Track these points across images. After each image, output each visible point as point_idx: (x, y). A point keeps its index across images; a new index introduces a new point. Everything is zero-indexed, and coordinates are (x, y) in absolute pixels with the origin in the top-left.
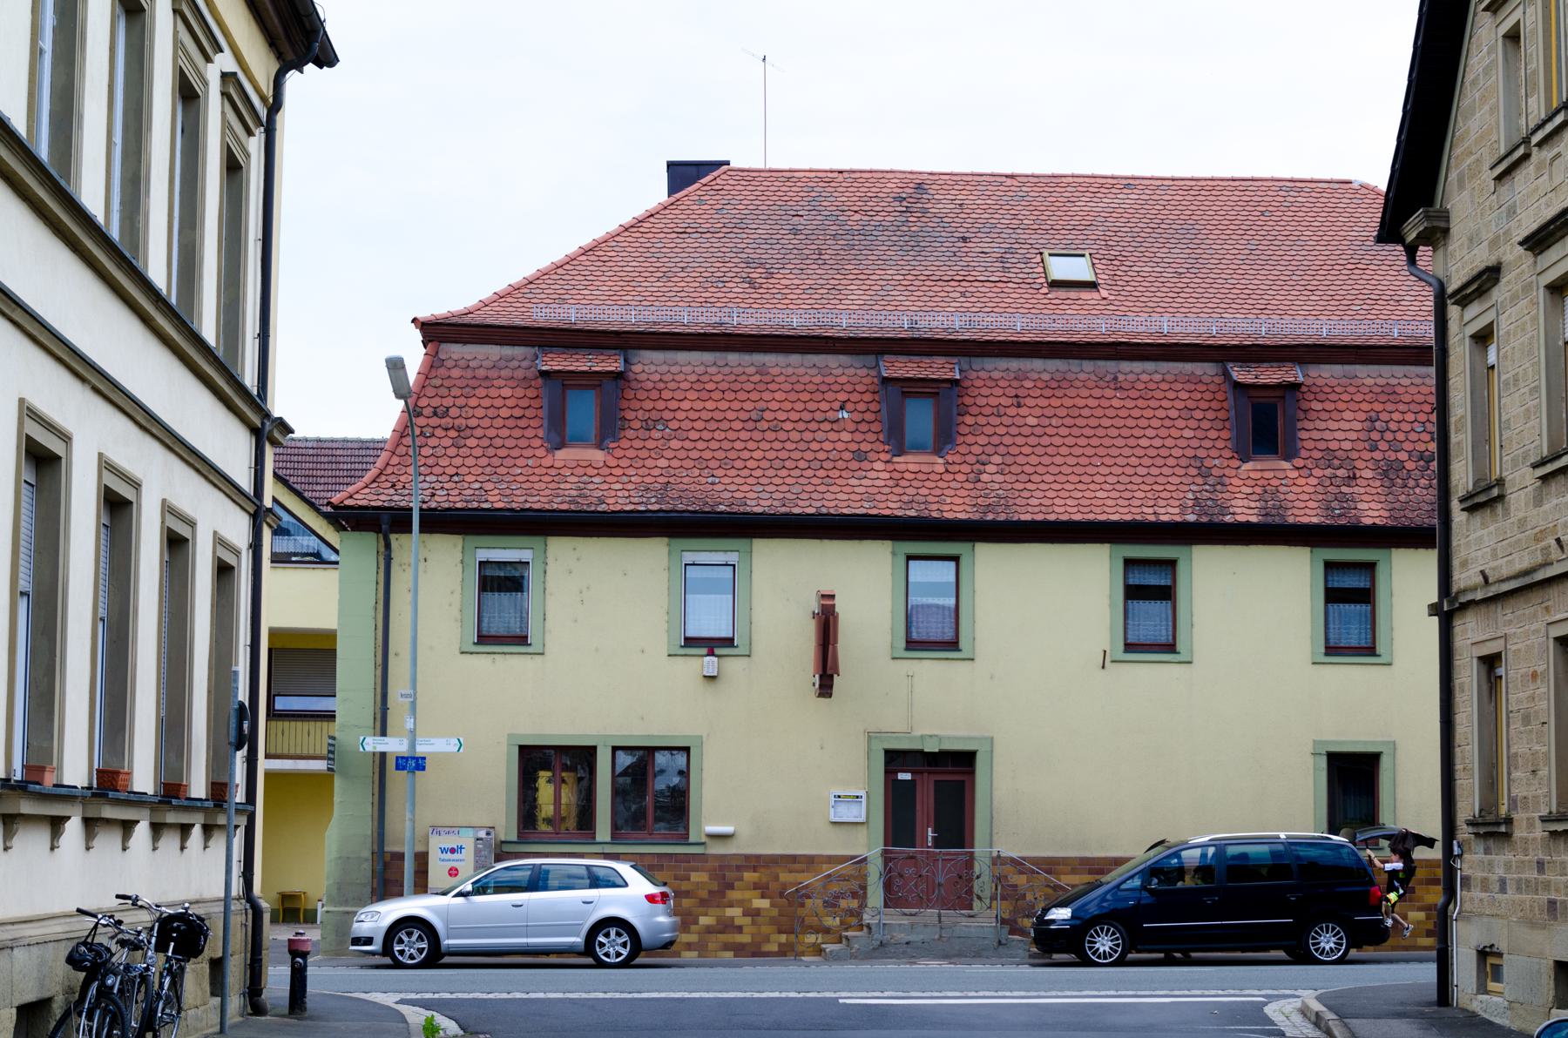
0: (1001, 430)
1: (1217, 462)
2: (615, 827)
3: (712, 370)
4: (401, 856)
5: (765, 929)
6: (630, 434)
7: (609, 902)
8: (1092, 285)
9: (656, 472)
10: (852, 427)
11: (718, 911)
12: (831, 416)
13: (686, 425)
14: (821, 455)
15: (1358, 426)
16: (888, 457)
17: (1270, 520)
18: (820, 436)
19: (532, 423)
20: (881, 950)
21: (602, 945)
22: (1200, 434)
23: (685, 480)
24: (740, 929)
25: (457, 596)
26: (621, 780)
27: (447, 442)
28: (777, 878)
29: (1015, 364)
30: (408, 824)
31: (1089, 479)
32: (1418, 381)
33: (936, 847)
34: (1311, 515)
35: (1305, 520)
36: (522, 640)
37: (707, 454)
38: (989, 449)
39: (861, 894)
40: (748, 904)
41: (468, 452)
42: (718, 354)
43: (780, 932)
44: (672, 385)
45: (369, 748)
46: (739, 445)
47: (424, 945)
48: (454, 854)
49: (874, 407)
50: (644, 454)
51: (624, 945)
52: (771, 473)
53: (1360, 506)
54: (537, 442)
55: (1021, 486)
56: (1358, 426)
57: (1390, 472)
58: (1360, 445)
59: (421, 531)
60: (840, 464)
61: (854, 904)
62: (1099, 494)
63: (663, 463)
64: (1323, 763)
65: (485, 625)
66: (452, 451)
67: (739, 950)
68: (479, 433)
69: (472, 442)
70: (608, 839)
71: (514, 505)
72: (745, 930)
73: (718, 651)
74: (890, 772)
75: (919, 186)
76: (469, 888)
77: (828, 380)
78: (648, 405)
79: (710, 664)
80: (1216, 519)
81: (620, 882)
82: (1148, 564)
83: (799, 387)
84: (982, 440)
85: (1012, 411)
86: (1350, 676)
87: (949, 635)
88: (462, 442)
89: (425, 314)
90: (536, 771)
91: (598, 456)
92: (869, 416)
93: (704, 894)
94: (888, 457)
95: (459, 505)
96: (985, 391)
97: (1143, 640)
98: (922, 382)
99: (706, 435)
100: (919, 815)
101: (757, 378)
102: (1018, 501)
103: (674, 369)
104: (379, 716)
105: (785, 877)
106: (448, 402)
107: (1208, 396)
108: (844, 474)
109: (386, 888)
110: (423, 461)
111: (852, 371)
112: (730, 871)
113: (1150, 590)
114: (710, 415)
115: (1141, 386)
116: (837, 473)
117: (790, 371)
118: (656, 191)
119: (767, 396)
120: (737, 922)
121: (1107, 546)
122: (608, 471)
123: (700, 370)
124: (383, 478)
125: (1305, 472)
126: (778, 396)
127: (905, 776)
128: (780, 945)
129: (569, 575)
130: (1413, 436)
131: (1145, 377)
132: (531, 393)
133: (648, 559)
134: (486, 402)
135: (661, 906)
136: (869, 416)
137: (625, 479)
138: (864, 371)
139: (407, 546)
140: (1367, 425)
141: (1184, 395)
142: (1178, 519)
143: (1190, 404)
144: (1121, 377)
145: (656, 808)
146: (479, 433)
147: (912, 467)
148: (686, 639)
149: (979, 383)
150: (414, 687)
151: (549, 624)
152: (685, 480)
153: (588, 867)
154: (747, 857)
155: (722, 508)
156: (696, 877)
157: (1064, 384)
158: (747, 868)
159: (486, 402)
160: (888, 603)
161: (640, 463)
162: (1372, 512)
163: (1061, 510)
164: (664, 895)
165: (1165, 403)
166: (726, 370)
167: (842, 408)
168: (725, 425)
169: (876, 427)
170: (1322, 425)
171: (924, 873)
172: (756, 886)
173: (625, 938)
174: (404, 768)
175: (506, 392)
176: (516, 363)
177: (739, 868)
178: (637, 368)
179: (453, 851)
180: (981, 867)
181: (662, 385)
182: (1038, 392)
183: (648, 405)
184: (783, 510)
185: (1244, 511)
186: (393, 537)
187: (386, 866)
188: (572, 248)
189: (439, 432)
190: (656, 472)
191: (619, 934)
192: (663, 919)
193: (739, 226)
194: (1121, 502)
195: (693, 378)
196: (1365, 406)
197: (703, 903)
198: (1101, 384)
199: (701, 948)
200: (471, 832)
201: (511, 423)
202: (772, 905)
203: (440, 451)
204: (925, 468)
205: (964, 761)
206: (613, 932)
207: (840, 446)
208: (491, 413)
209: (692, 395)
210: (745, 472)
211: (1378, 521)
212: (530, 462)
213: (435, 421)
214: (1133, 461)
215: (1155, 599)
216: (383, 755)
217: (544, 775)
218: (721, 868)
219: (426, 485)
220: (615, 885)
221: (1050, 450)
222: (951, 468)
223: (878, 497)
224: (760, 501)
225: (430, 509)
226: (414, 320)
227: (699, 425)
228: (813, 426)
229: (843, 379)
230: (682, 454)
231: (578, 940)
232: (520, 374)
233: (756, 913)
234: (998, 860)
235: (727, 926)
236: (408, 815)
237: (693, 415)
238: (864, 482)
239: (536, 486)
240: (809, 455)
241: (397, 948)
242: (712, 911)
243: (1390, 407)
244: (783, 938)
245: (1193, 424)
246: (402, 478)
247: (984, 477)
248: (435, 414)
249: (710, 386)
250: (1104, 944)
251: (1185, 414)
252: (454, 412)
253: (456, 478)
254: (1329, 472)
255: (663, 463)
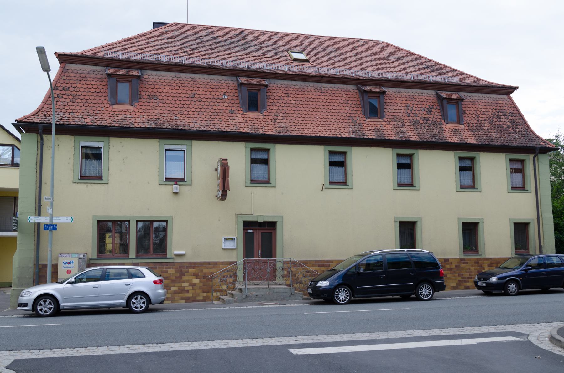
0: (283, 105)
1: (358, 118)
2: (138, 252)
3: (175, 79)
4: (46, 266)
5: (198, 291)
6: (143, 100)
7: (137, 285)
8: (307, 61)
9: (154, 114)
10: (228, 101)
11: (179, 285)
12: (220, 97)
13: (165, 98)
14: (217, 111)
15: (403, 108)
16: (242, 112)
17: (379, 138)
18: (216, 104)
19: (104, 94)
20: (246, 299)
21: (134, 303)
22: (351, 109)
23: (165, 118)
24: (187, 291)
25: (72, 161)
26: (139, 234)
27: (68, 100)
28: (202, 271)
29: (286, 82)
30: (49, 252)
31: (315, 123)
32: (421, 94)
33: (262, 257)
34: (392, 136)
35: (391, 138)
36: (99, 178)
37: (174, 109)
38: (279, 111)
39: (235, 276)
40: (191, 281)
41: (77, 104)
42: (177, 73)
43: (204, 292)
44: (159, 83)
45: (32, 221)
46: (186, 106)
47: (52, 306)
48: (69, 265)
49: (236, 95)
50: (149, 108)
51: (144, 303)
52: (199, 116)
53: (408, 134)
54: (106, 102)
55: (291, 124)
56: (403, 108)
57: (415, 124)
58: (405, 115)
59: (56, 134)
60: (224, 114)
61: (231, 280)
62: (319, 128)
63: (156, 111)
64: (398, 224)
65: (83, 172)
66: (71, 104)
67: (187, 300)
68: (82, 97)
69: (79, 101)
70: (134, 257)
71: (96, 124)
72: (190, 292)
73: (179, 183)
74: (245, 230)
75: (242, 32)
76: (73, 280)
77: (218, 84)
78: (150, 90)
79: (176, 188)
80: (362, 137)
81: (140, 275)
82: (338, 151)
83: (208, 86)
84: (276, 108)
85: (286, 98)
86: (406, 194)
87: (266, 178)
88: (75, 100)
89: (60, 51)
90: (104, 234)
91: (130, 108)
92: (234, 98)
93: (173, 278)
94: (242, 112)
95: (72, 123)
96: (276, 91)
97: (335, 181)
98: (253, 88)
99: (173, 102)
100: (255, 245)
101: (192, 82)
102: (291, 129)
103: (160, 78)
104: (37, 208)
105: (205, 270)
106: (69, 85)
107: (353, 96)
108: (226, 118)
109: (39, 280)
110: (58, 107)
111: (227, 82)
112: (184, 269)
113: (337, 163)
114: (174, 95)
115: (330, 92)
116: (224, 117)
117: (204, 80)
118: (150, 28)
119: (196, 89)
120: (187, 289)
121: (323, 146)
122: (135, 113)
123: (171, 78)
124: (41, 113)
125: (387, 123)
126: (200, 89)
127: (250, 231)
128: (204, 297)
129: (117, 151)
130: (421, 112)
131: (331, 89)
132: (103, 83)
133: (150, 148)
134: (85, 86)
135: (159, 285)
136: (234, 98)
137: (141, 116)
138: (232, 82)
139: (51, 139)
140: (406, 108)
141: (345, 96)
142: (348, 136)
143: (347, 99)
144: (323, 89)
145: (154, 244)
146: (82, 97)
147: (251, 116)
148: (166, 178)
149: (273, 88)
150: (52, 196)
151: (110, 172)
152: (165, 118)
153: (127, 269)
154: (191, 263)
155: (180, 128)
156: (170, 271)
157: (304, 90)
158: (190, 267)
159: (85, 86)
160: (244, 166)
161: (147, 111)
162: (413, 137)
163: (307, 132)
164: (161, 280)
165: (339, 98)
166: (180, 79)
167: (224, 95)
168: (180, 99)
169: (237, 102)
170: (392, 108)
171: (262, 268)
172: (194, 274)
173: (144, 300)
174: (47, 229)
175: (93, 83)
176: (97, 73)
177: (187, 267)
178: (146, 77)
179: (69, 263)
180: (279, 265)
181: (155, 83)
182: (295, 92)
183: (150, 90)
184: (204, 129)
185: (370, 135)
186: (44, 136)
187: (40, 269)
188: (120, 39)
189: (65, 96)
190: (154, 114)
191: (141, 298)
192: (161, 291)
193: (181, 37)
194: (327, 130)
195: (168, 81)
196: (405, 102)
197: (173, 281)
198: (316, 90)
199: (172, 299)
200: (77, 255)
201: (95, 94)
202: (200, 282)
203: (65, 104)
204: (256, 117)
205: (272, 225)
206: (139, 297)
207: (224, 108)
208: (87, 90)
209: (167, 87)
210: (189, 116)
211: (415, 139)
212: (103, 109)
213: (63, 92)
214: (329, 117)
215: (339, 166)
216: (39, 224)
217: (108, 235)
218: (180, 267)
219: (59, 116)
220: (139, 277)
221: (300, 112)
222: (265, 117)
223: (240, 126)
224: (195, 125)
225: (60, 124)
226: (55, 53)
227: (170, 98)
228: (214, 100)
229: (224, 84)
230: (164, 108)
231: (123, 301)
232: (99, 76)
233: (194, 285)
234: (285, 263)
235: (183, 290)
236: (49, 249)
237: (167, 94)
238: (234, 121)
239: (105, 118)
240: (213, 111)
241: (39, 308)
242: (176, 284)
243: (413, 102)
244: (205, 294)
245: (348, 105)
246: (49, 113)
247: (278, 121)
248: (64, 89)
249: (174, 84)
250: (342, 295)
251: (345, 102)
252: (71, 89)
253: (72, 114)
254: (395, 123)
255: (156, 111)
